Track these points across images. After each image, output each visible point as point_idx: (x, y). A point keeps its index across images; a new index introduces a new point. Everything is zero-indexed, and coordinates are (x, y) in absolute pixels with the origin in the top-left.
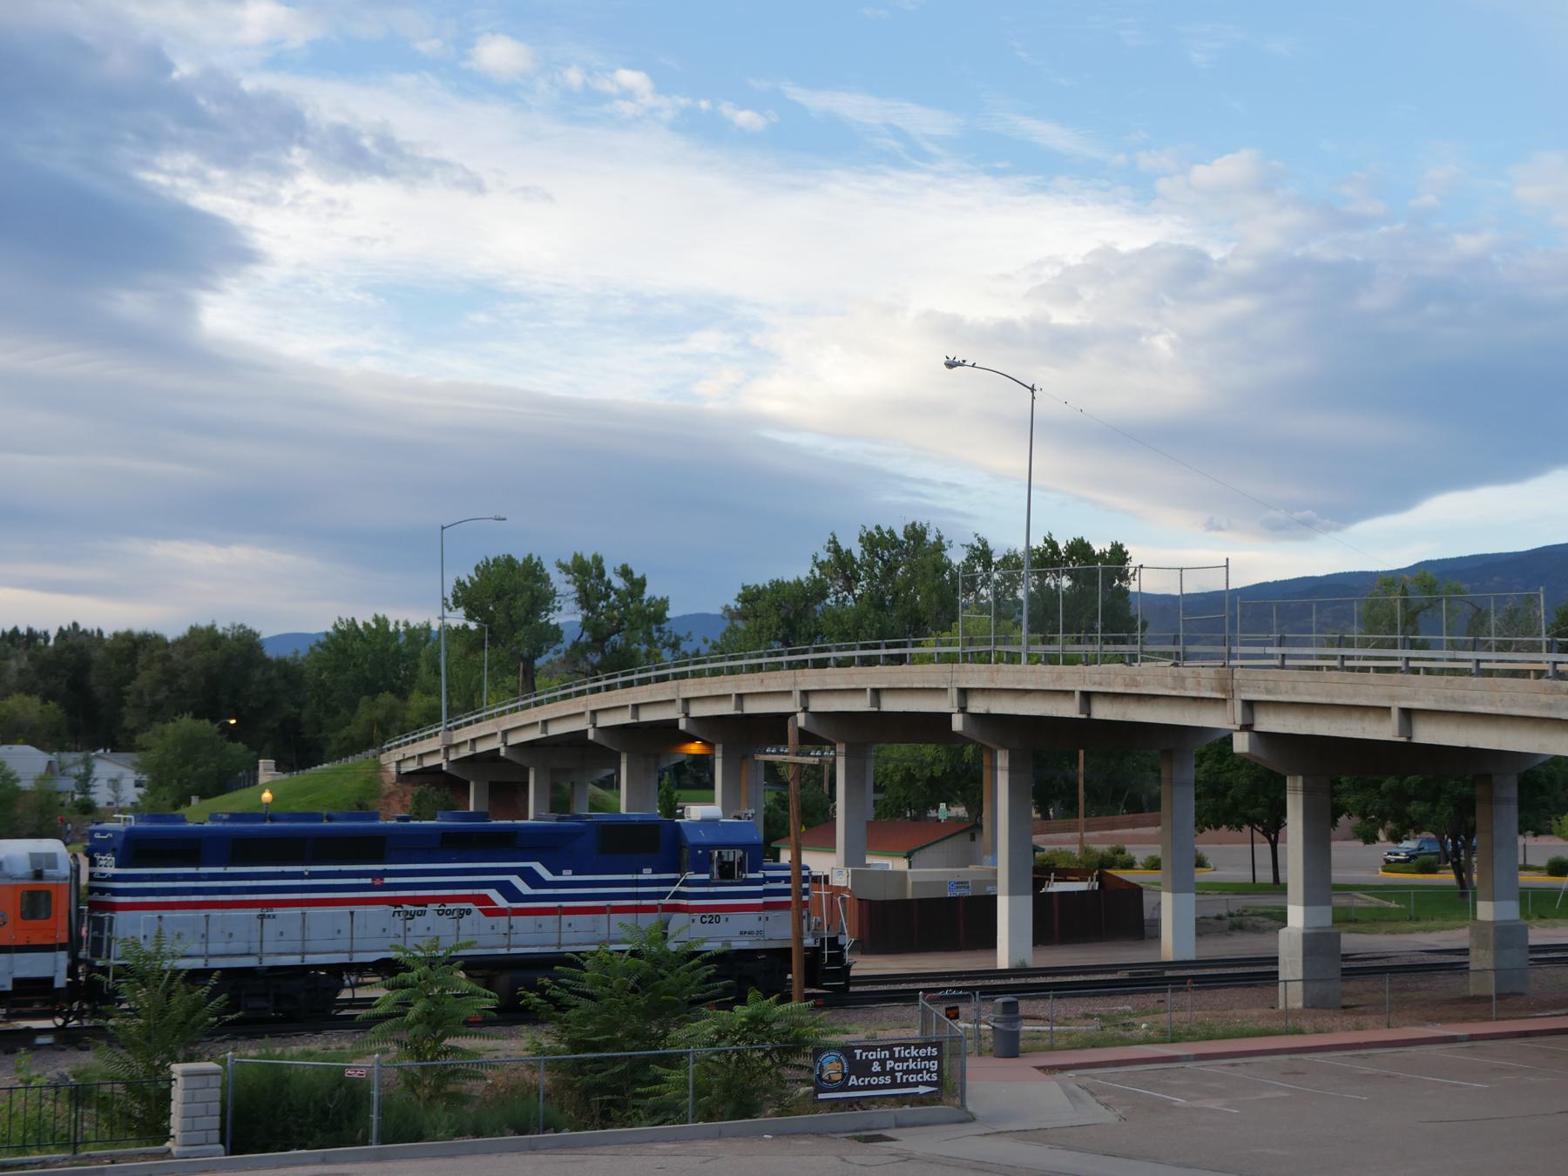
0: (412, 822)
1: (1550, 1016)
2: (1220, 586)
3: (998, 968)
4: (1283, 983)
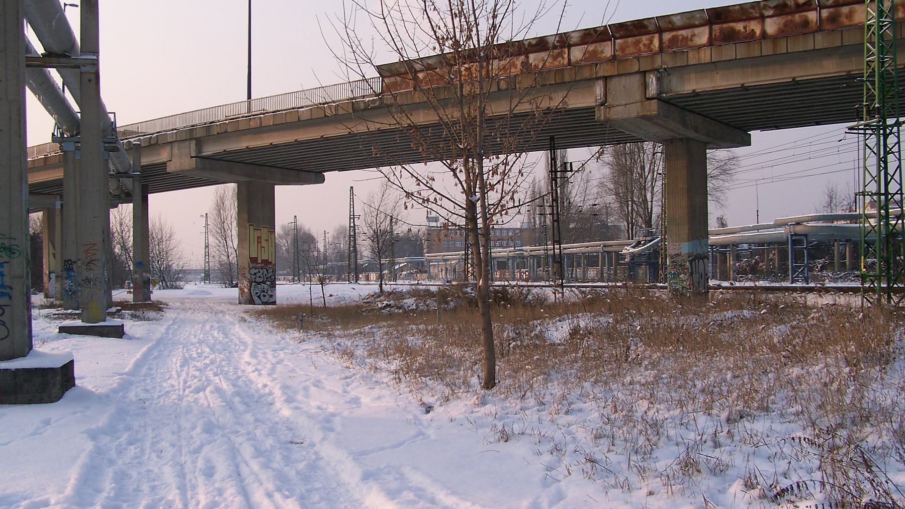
3: (33, 322)
4: (845, 34)
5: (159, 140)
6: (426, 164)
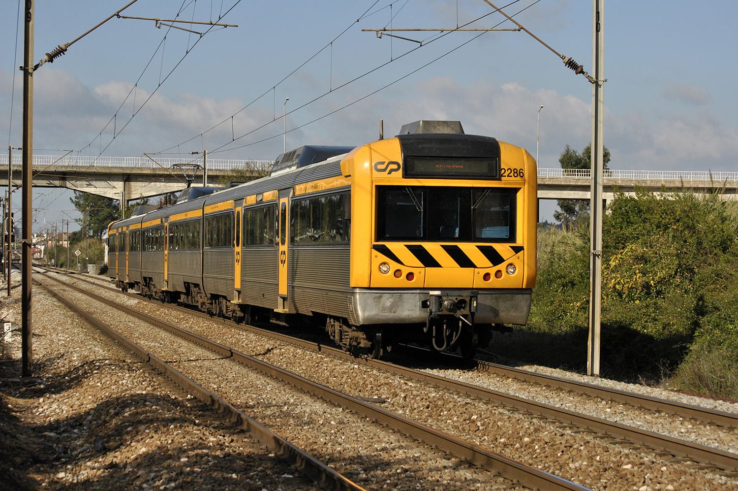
0: (273, 175)
1: (485, 294)
2: (33, 192)
5: (13, 163)
6: (47, 54)
